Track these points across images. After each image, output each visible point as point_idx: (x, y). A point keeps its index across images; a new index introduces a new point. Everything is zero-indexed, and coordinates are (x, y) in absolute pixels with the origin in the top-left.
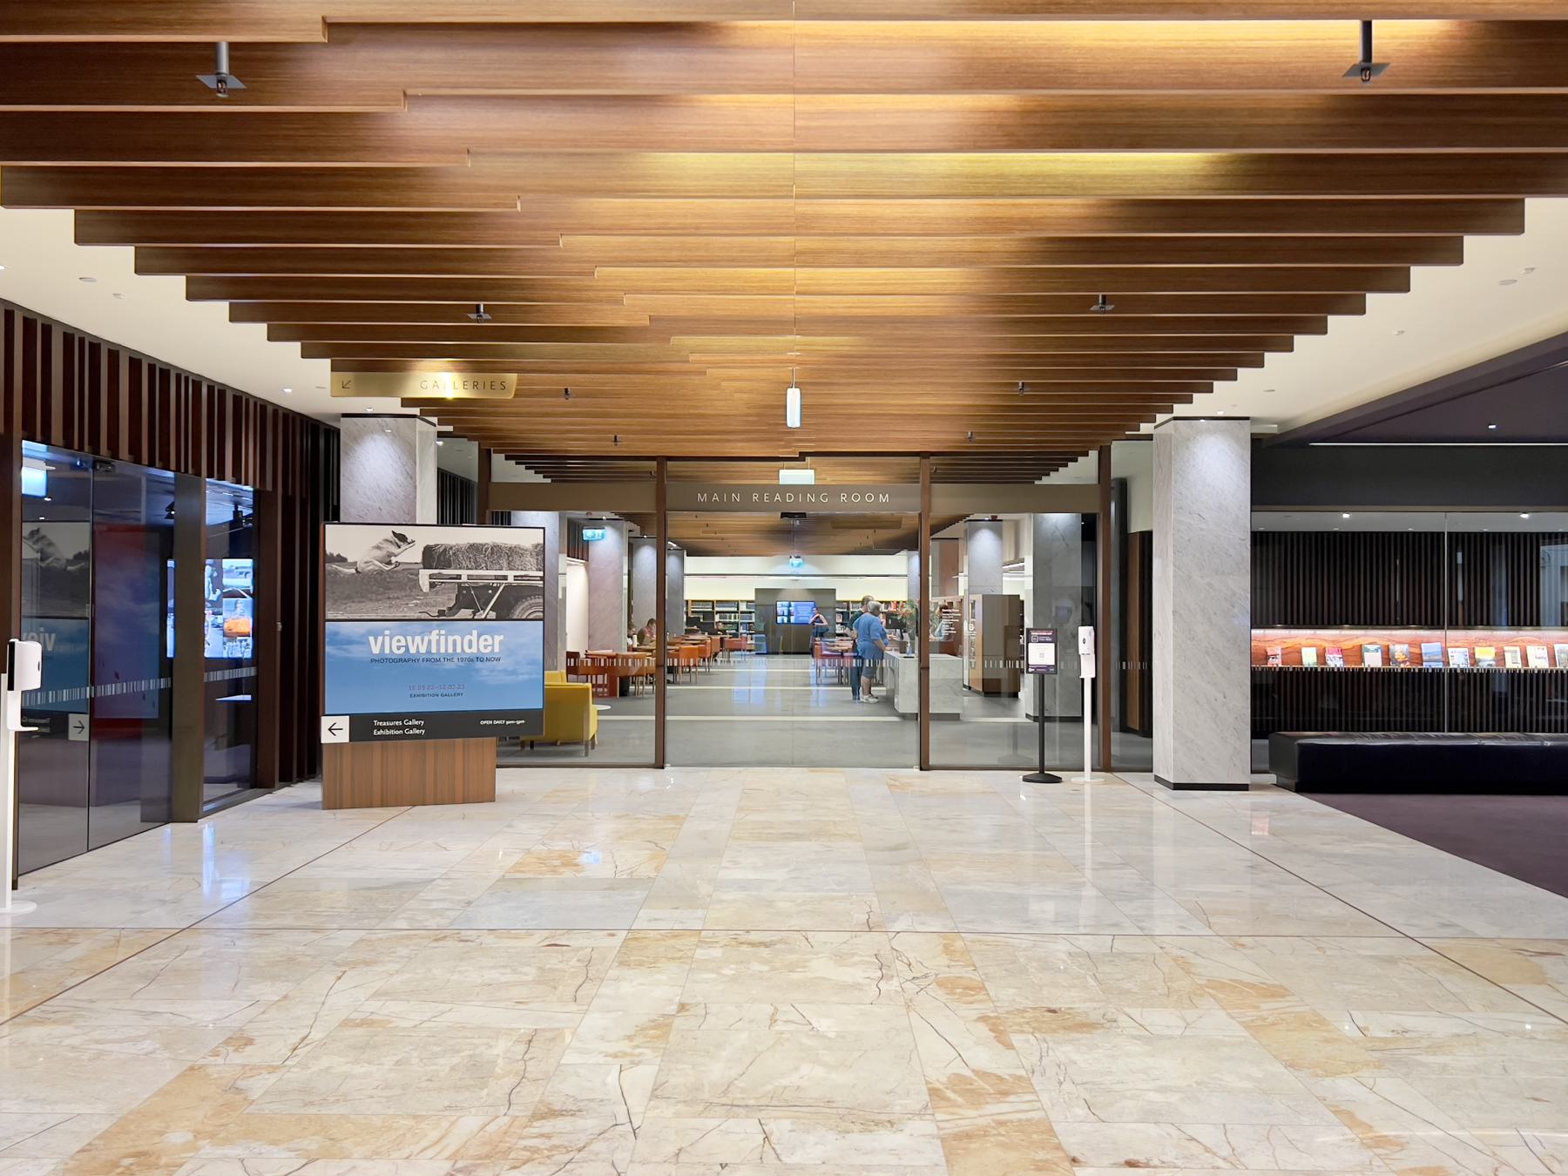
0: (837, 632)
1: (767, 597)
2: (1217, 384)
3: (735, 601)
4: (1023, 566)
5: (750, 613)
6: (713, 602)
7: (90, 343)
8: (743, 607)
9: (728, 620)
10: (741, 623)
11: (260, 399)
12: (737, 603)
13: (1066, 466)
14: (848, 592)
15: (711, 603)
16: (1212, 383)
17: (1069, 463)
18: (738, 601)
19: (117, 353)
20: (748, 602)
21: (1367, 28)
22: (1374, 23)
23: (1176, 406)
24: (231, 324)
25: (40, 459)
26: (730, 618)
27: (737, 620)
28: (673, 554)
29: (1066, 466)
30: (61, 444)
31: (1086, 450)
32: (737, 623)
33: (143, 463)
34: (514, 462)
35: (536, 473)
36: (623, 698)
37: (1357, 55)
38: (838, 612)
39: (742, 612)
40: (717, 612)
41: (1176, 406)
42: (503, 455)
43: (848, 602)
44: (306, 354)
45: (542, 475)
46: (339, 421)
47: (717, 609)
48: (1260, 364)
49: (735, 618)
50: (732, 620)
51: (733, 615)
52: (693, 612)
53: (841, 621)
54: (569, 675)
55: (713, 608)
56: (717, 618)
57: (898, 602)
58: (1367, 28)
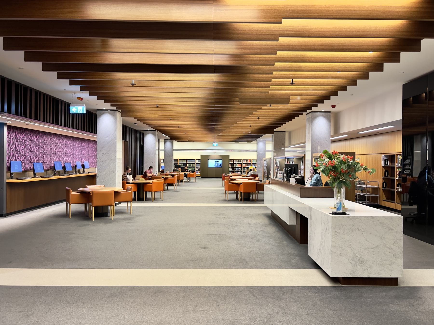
0: (230, 170)
1: (205, 159)
2: (296, 117)
3: (194, 159)
4: (305, 145)
5: (199, 163)
6: (186, 160)
7: (91, 113)
8: (197, 162)
9: (191, 166)
10: (196, 167)
11: (67, 102)
12: (194, 160)
13: (294, 118)
14: (233, 156)
15: (185, 160)
16: (312, 108)
17: (292, 119)
18: (195, 159)
19: (54, 99)
20: (198, 160)
21: (292, 80)
22: (293, 80)
23: (313, 108)
24: (43, 71)
25: (281, 179)
26: (192, 165)
27: (195, 166)
28: (168, 141)
29: (294, 118)
30: (15, 114)
31: (356, 79)
32: (195, 167)
33: (48, 122)
34: (103, 101)
35: (151, 127)
36: (100, 220)
37: (291, 82)
38: (230, 163)
39: (196, 163)
40: (188, 163)
41: (313, 108)
42: (103, 101)
43: (233, 160)
44: (45, 68)
45: (153, 128)
46: (96, 111)
47: (188, 162)
48: (295, 118)
49: (194, 165)
50: (193, 166)
51: (193, 164)
52: (179, 163)
53: (231, 166)
54: (429, 101)
55: (186, 162)
56: (188, 165)
57: (251, 160)
58: (292, 80)
